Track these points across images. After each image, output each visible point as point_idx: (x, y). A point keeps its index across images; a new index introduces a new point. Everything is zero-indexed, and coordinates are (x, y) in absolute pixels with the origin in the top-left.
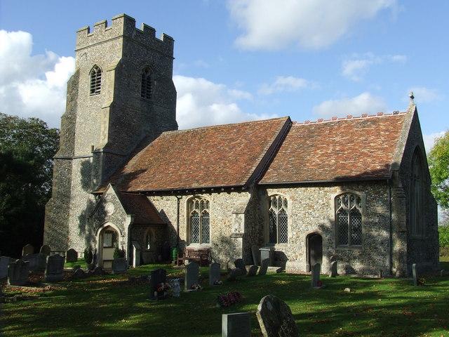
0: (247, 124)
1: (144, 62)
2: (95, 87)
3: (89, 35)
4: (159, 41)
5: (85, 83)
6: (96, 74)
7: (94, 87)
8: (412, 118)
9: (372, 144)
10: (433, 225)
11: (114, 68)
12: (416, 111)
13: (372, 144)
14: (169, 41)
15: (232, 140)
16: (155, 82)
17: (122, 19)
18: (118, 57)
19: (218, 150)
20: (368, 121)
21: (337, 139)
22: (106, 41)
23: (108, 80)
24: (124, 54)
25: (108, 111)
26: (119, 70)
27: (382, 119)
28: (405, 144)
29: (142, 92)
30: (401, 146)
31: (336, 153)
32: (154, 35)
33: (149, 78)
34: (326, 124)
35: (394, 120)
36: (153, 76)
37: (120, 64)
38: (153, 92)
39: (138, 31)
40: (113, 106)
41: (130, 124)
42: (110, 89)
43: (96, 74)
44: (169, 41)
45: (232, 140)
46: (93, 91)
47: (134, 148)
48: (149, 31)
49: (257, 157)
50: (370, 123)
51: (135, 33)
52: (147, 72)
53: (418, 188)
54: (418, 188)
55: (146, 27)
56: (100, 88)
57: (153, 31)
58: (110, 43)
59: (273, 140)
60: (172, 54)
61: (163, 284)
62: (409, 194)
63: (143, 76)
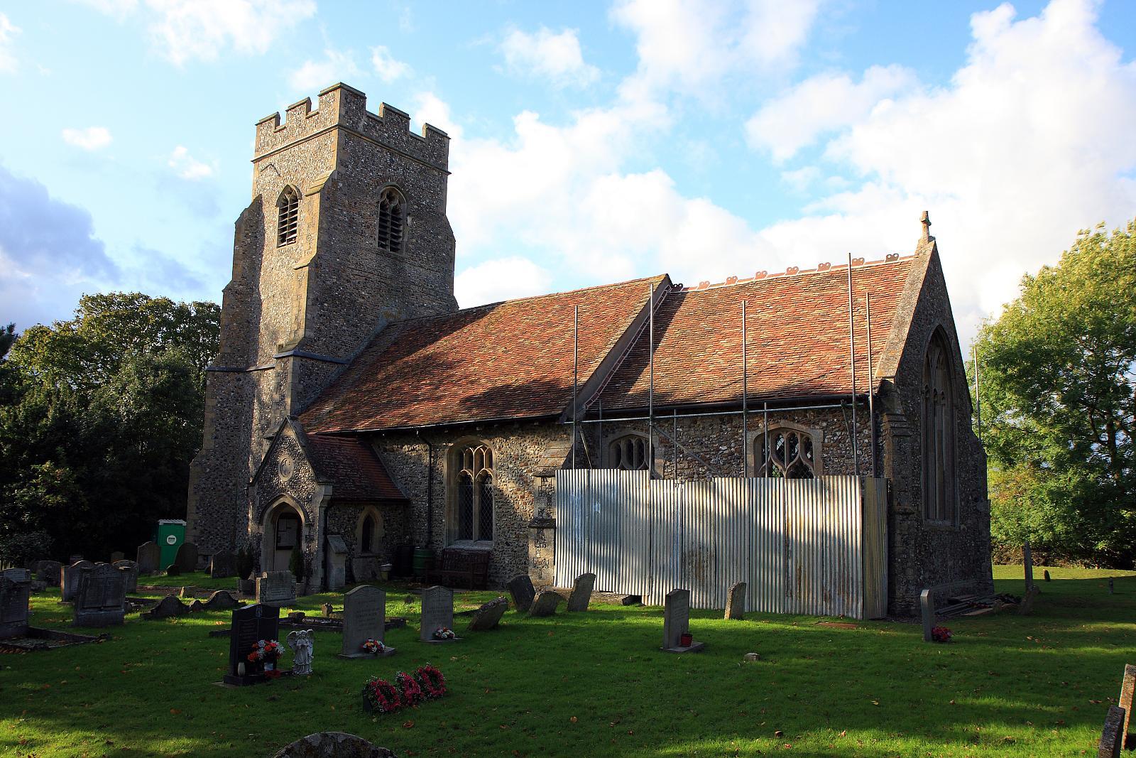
0: (584, 293)
1: (383, 179)
2: (287, 233)
3: (278, 128)
4: (416, 138)
5: (272, 216)
6: (288, 203)
7: (284, 229)
8: (926, 265)
9: (838, 324)
10: (976, 500)
11: (319, 188)
12: (935, 254)
13: (838, 324)
14: (437, 138)
15: (550, 325)
16: (408, 218)
17: (338, 94)
18: (326, 166)
19: (520, 346)
20: (831, 276)
21: (765, 316)
22: (307, 139)
23: (309, 214)
24: (340, 162)
25: (306, 274)
26: (330, 194)
27: (862, 271)
28: (909, 319)
29: (380, 238)
30: (902, 324)
31: (762, 345)
32: (364, 106)
33: (395, 211)
34: (743, 287)
35: (891, 268)
36: (404, 206)
37: (332, 181)
38: (405, 237)
39: (371, 117)
40: (315, 265)
41: (353, 302)
42: (311, 231)
43: (288, 203)
44: (437, 138)
45: (550, 325)
46: (283, 238)
47: (362, 348)
48: (397, 119)
49: (593, 358)
50: (830, 283)
51: (364, 121)
52: (390, 198)
53: (942, 420)
54: (942, 420)
55: (388, 109)
56: (295, 232)
57: (404, 118)
58: (313, 144)
59: (630, 321)
60: (446, 164)
61: (112, 449)
62: (922, 432)
63: (383, 206)
